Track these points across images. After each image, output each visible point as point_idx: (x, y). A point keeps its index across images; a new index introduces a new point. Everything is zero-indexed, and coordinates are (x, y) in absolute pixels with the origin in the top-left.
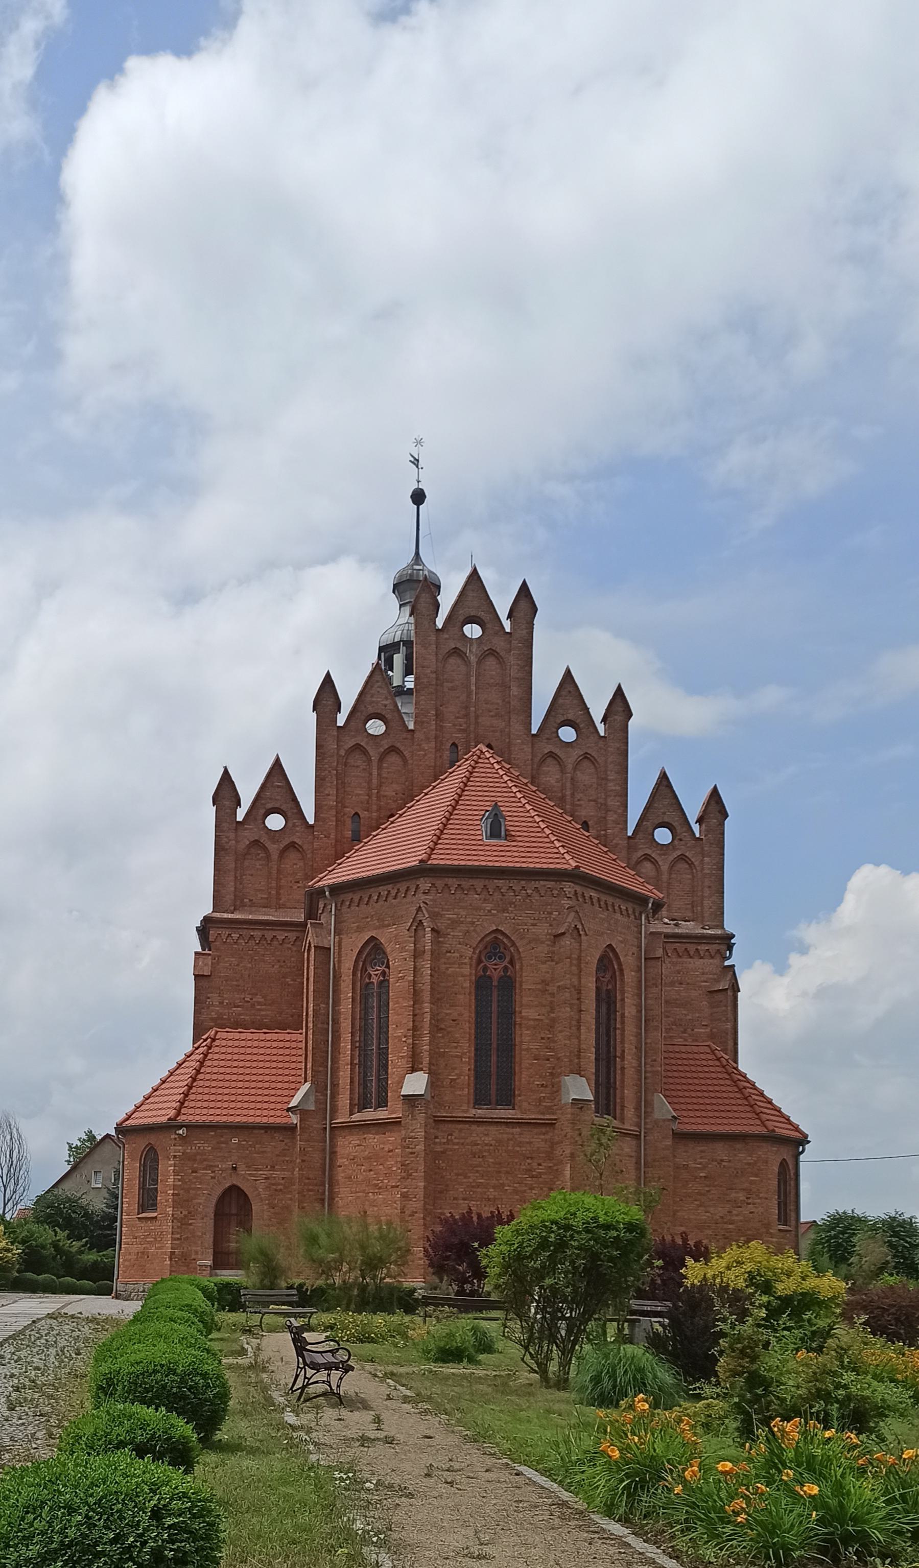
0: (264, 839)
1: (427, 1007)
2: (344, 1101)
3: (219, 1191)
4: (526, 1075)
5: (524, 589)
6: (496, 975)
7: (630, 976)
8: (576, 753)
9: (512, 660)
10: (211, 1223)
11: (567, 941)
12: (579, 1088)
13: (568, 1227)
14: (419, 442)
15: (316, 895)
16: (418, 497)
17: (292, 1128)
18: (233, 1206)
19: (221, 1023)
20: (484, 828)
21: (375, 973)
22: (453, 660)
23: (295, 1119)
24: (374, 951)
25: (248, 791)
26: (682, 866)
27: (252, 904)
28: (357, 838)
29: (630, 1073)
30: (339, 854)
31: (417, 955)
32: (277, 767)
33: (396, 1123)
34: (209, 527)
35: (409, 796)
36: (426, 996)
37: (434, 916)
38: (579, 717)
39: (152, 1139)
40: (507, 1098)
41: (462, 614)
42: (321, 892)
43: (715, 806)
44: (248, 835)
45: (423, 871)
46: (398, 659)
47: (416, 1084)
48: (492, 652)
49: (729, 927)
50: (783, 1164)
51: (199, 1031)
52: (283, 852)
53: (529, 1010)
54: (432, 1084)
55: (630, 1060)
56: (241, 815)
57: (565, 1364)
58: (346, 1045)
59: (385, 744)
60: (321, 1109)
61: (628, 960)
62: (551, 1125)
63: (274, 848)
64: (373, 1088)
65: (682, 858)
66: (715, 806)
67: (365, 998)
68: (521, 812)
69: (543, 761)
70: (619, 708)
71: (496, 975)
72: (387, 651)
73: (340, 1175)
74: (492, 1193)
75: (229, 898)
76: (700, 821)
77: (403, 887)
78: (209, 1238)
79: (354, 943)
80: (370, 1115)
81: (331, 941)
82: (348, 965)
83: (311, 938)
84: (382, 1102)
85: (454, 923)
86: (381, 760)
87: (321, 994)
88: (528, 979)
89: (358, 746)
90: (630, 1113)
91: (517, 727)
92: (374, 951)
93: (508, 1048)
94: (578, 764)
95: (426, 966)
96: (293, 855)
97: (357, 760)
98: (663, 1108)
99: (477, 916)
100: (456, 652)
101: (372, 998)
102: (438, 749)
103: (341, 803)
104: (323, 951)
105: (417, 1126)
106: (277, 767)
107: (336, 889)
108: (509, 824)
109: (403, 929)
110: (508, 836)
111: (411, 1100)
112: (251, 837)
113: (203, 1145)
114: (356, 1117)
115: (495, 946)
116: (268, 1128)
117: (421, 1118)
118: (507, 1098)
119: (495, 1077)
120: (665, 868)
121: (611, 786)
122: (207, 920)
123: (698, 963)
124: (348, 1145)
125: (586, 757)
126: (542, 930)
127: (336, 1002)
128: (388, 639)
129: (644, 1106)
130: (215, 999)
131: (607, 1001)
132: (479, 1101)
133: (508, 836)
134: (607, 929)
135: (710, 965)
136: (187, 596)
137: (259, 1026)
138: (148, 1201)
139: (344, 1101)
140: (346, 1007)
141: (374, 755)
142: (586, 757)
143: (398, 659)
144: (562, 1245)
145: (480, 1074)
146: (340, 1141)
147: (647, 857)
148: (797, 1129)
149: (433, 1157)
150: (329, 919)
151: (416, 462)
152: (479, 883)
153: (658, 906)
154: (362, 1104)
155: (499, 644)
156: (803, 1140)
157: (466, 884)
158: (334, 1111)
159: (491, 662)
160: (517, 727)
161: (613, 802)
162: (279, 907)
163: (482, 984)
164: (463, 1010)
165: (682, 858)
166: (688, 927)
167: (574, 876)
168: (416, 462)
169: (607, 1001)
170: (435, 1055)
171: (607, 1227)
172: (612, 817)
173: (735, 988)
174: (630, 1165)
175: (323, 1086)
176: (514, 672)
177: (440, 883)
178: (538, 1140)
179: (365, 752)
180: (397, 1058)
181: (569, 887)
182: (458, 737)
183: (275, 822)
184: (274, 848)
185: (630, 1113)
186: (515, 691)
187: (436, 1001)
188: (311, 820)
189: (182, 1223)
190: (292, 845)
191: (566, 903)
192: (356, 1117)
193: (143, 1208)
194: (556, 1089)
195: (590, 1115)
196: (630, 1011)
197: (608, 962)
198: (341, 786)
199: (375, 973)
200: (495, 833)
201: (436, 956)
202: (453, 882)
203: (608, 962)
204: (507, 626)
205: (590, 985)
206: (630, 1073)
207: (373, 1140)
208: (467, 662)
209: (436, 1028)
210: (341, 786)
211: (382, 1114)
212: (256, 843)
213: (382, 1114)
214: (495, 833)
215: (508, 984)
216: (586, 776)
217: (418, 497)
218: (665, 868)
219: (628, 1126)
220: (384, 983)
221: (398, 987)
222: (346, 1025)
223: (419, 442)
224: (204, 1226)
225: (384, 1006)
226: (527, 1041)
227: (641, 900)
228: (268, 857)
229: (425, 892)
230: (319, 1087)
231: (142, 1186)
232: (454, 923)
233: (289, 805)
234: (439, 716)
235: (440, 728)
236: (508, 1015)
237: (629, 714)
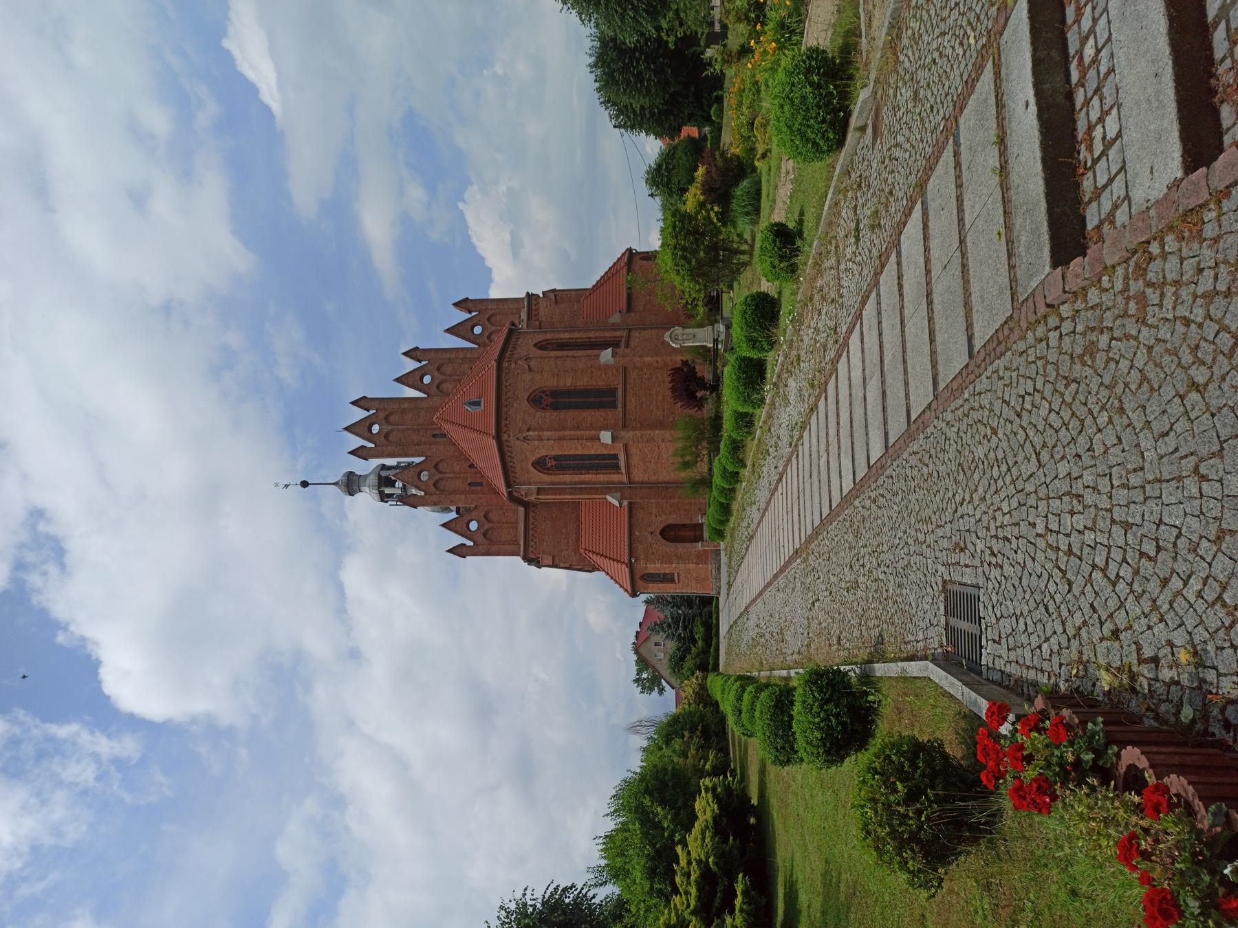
0: (482, 531)
1: (567, 433)
2: (615, 478)
3: (664, 541)
4: (600, 382)
6: (550, 400)
7: (549, 336)
8: (436, 374)
10: (680, 545)
11: (532, 364)
12: (606, 355)
13: (675, 248)
14: (277, 485)
16: (305, 484)
17: (630, 504)
18: (671, 534)
21: (550, 463)
22: (391, 438)
23: (625, 503)
24: (540, 464)
25: (457, 540)
26: (493, 320)
27: (516, 536)
29: (597, 334)
31: (540, 439)
32: (444, 525)
33: (626, 446)
34: (318, 643)
35: (462, 456)
36: (561, 433)
37: (521, 431)
38: (420, 373)
39: (637, 577)
40: (612, 392)
41: (367, 434)
42: (510, 493)
43: (462, 304)
44: (480, 539)
45: (498, 437)
46: (388, 491)
47: (606, 437)
48: (386, 418)
49: (523, 295)
50: (642, 259)
53: (568, 382)
54: (606, 429)
55: (591, 334)
57: (743, 253)
58: (586, 477)
59: (433, 470)
60: (617, 490)
61: (541, 337)
62: (625, 369)
64: (608, 462)
65: (489, 319)
66: (462, 304)
69: (437, 488)
70: (413, 354)
72: (384, 498)
73: (653, 479)
74: (660, 397)
75: (513, 547)
76: (470, 312)
77: (506, 449)
78: (687, 545)
79: (535, 475)
80: (622, 463)
81: (534, 487)
82: (546, 478)
83: (532, 498)
84: (615, 457)
85: (524, 421)
87: (561, 491)
90: (618, 334)
91: (424, 404)
92: (540, 464)
93: (587, 393)
94: (443, 374)
95: (547, 434)
96: (491, 516)
97: (441, 485)
98: (616, 318)
99: (521, 411)
100: (386, 436)
101: (563, 464)
102: (435, 444)
104: (539, 491)
105: (627, 435)
106: (444, 525)
107: (508, 485)
111: (614, 439)
113: (640, 549)
114: (623, 470)
115: (536, 400)
116: (630, 517)
117: (623, 433)
118: (612, 392)
119: (601, 398)
121: (453, 356)
123: (541, 309)
124: (638, 475)
125: (438, 369)
126: (527, 377)
127: (566, 484)
128: (377, 497)
129: (615, 327)
131: (562, 346)
132: (615, 407)
134: (526, 346)
135: (542, 304)
136: (354, 655)
137: (578, 528)
138: (668, 578)
139: (615, 478)
140: (567, 478)
142: (438, 369)
143: (388, 491)
144: (684, 249)
145: (601, 406)
146: (637, 479)
147: (489, 337)
148: (623, 254)
149: (642, 427)
151: (287, 486)
152: (504, 410)
153: (513, 324)
154: (616, 468)
155: (382, 415)
156: (630, 250)
157: (504, 416)
158: (621, 483)
159: (391, 419)
160: (424, 404)
161: (461, 355)
162: (517, 522)
163: (555, 407)
164: (568, 416)
165: (489, 319)
166: (524, 315)
167: (500, 361)
168: (287, 486)
169: (562, 346)
170: (591, 428)
171: (674, 227)
172: (469, 355)
173: (554, 291)
174: (644, 333)
175: (608, 488)
176: (396, 406)
178: (633, 376)
181: (505, 365)
185: (618, 334)
186: (406, 406)
187: (564, 429)
189: (680, 559)
190: (485, 516)
191: (513, 366)
192: (623, 470)
193: (673, 581)
194: (607, 367)
195: (620, 350)
196: (566, 335)
197: (542, 346)
199: (550, 463)
201: (541, 430)
202: (503, 422)
203: (542, 346)
204: (372, 412)
205: (553, 353)
207: (635, 460)
208: (392, 431)
209: (578, 428)
211: (622, 457)
212: (484, 535)
213: (622, 457)
215: (555, 393)
216: (448, 369)
217: (305, 484)
218: (494, 328)
219: (625, 334)
220: (555, 458)
222: (577, 478)
223: (277, 485)
224: (681, 548)
226: (583, 382)
227: (511, 332)
228: (491, 528)
230: (609, 491)
231: (662, 582)
232: (524, 421)
234: (418, 444)
235: (425, 443)
236: (570, 393)
237: (417, 348)
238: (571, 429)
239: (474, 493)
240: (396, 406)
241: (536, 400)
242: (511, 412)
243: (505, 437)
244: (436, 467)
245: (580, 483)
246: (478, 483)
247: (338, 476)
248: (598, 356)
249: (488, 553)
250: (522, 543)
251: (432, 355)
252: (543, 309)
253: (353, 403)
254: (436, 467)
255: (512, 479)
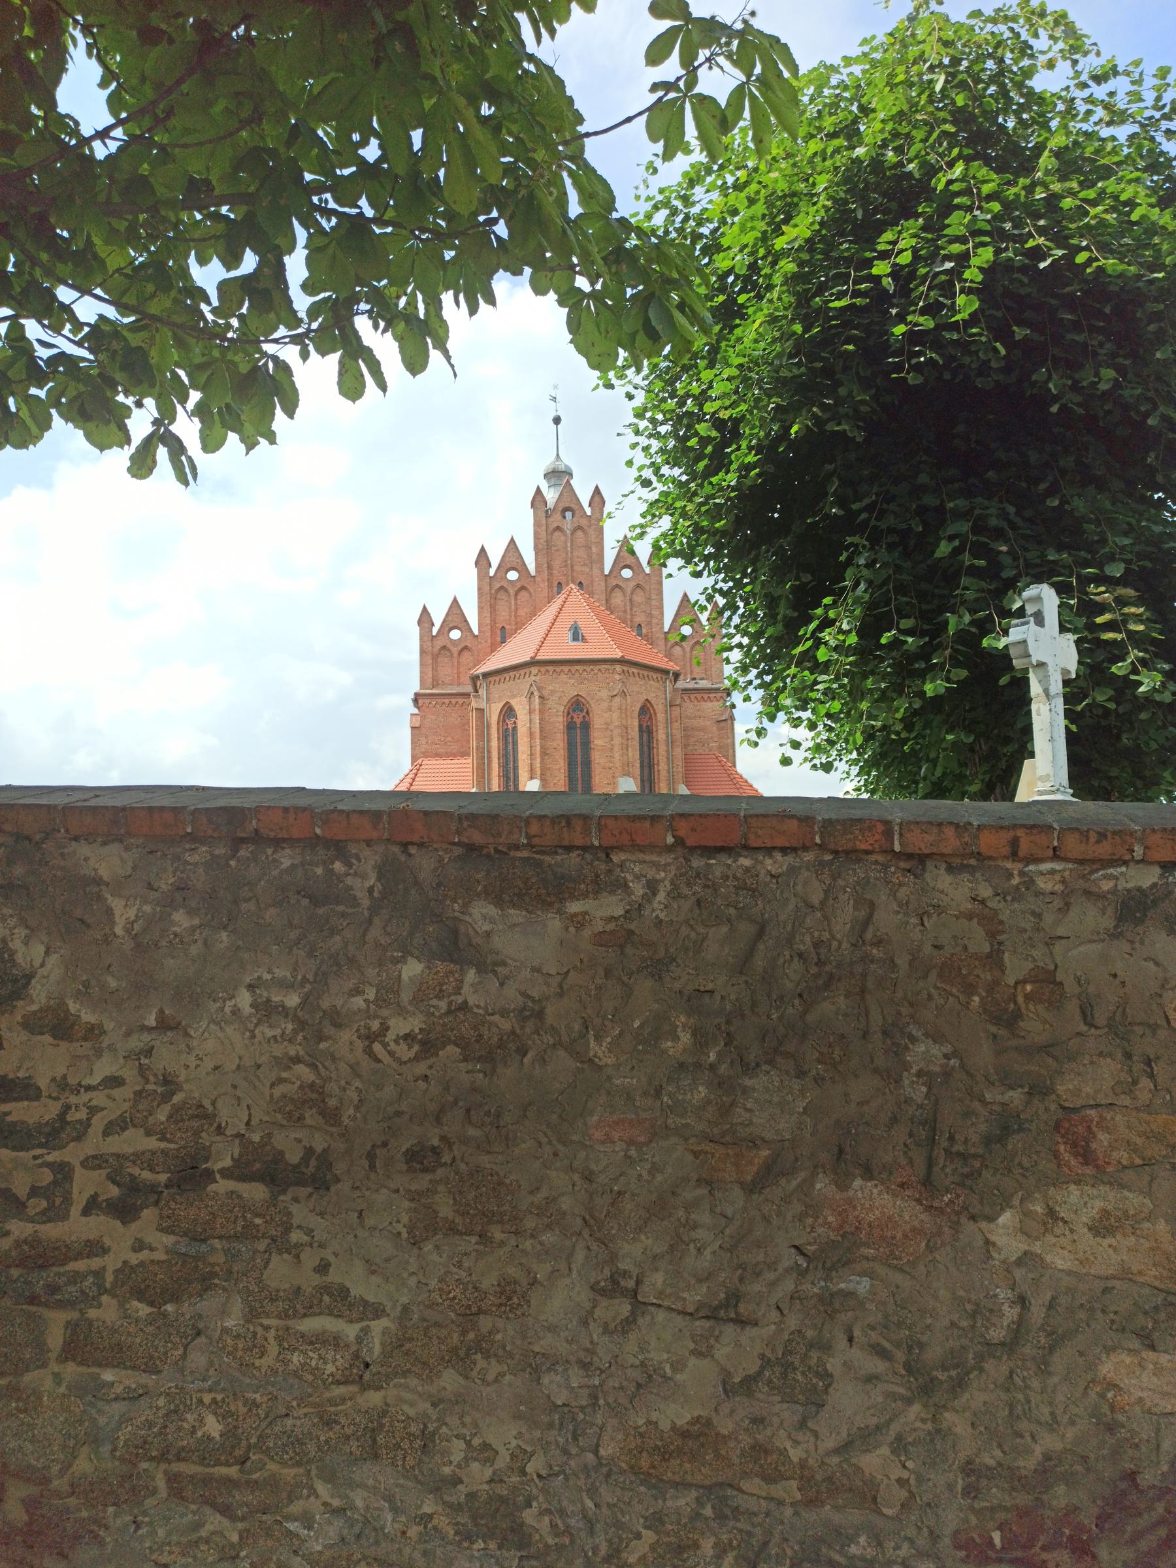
1: (538, 741)
5: (597, 491)
6: (578, 721)
7: (661, 717)
9: (591, 532)
11: (617, 699)
14: (556, 387)
15: (474, 679)
16: (557, 420)
19: (426, 755)
20: (570, 635)
22: (556, 534)
24: (508, 712)
28: (503, 641)
29: (663, 773)
30: (493, 648)
31: (531, 712)
35: (533, 614)
36: (537, 735)
37: (539, 689)
38: (636, 566)
44: (439, 644)
45: (533, 663)
48: (580, 528)
51: (414, 758)
52: (460, 652)
53: (598, 740)
56: (435, 631)
59: (519, 585)
61: (659, 708)
63: (455, 651)
67: (505, 737)
68: (591, 625)
71: (578, 721)
77: (522, 672)
81: (483, 705)
85: (553, 692)
86: (516, 595)
87: (480, 736)
88: (597, 722)
89: (502, 588)
91: (596, 571)
93: (587, 763)
95: (536, 718)
96: (466, 654)
97: (502, 595)
99: (564, 688)
101: (508, 737)
103: (493, 621)
104: (481, 711)
107: (486, 675)
108: (584, 630)
109: (524, 700)
110: (584, 639)
112: (440, 645)
115: (577, 705)
120: (688, 649)
122: (416, 695)
123: (709, 705)
126: (604, 694)
130: (423, 740)
131: (647, 732)
133: (584, 639)
135: (717, 705)
140: (494, 743)
141: (512, 591)
142: (638, 586)
150: (483, 692)
151: (554, 399)
152: (566, 668)
157: (558, 669)
161: (655, 612)
163: (570, 727)
164: (559, 743)
166: (703, 684)
168: (554, 399)
169: (647, 732)
172: (655, 621)
176: (593, 539)
177: (543, 669)
179: (507, 591)
180: (523, 773)
181: (618, 668)
182: (562, 579)
183: (455, 635)
184: (455, 651)
186: (594, 549)
187: (543, 738)
188: (476, 632)
190: (466, 648)
197: (646, 710)
198: (493, 609)
200: (575, 638)
201: (541, 712)
206: (663, 773)
210: (493, 609)
212: (444, 647)
214: (575, 638)
215: (586, 726)
220: (515, 728)
221: (522, 731)
225: (515, 743)
226: (597, 757)
227: (666, 672)
229: (533, 676)
232: (553, 692)
233: (463, 624)
234: (549, 567)
235: (550, 574)
236: (587, 745)
238: (542, 747)
239: (493, 633)
240: (593, 539)
241: (577, 705)
242: (563, 677)
243: (534, 670)
244: (523, 588)
245: (489, 758)
246: (501, 635)
247: (568, 460)
248: (628, 774)
249: (423, 652)
250: (434, 691)
251: (654, 579)
252: (712, 707)
253: (597, 488)
254: (523, 588)
255: (492, 679)
